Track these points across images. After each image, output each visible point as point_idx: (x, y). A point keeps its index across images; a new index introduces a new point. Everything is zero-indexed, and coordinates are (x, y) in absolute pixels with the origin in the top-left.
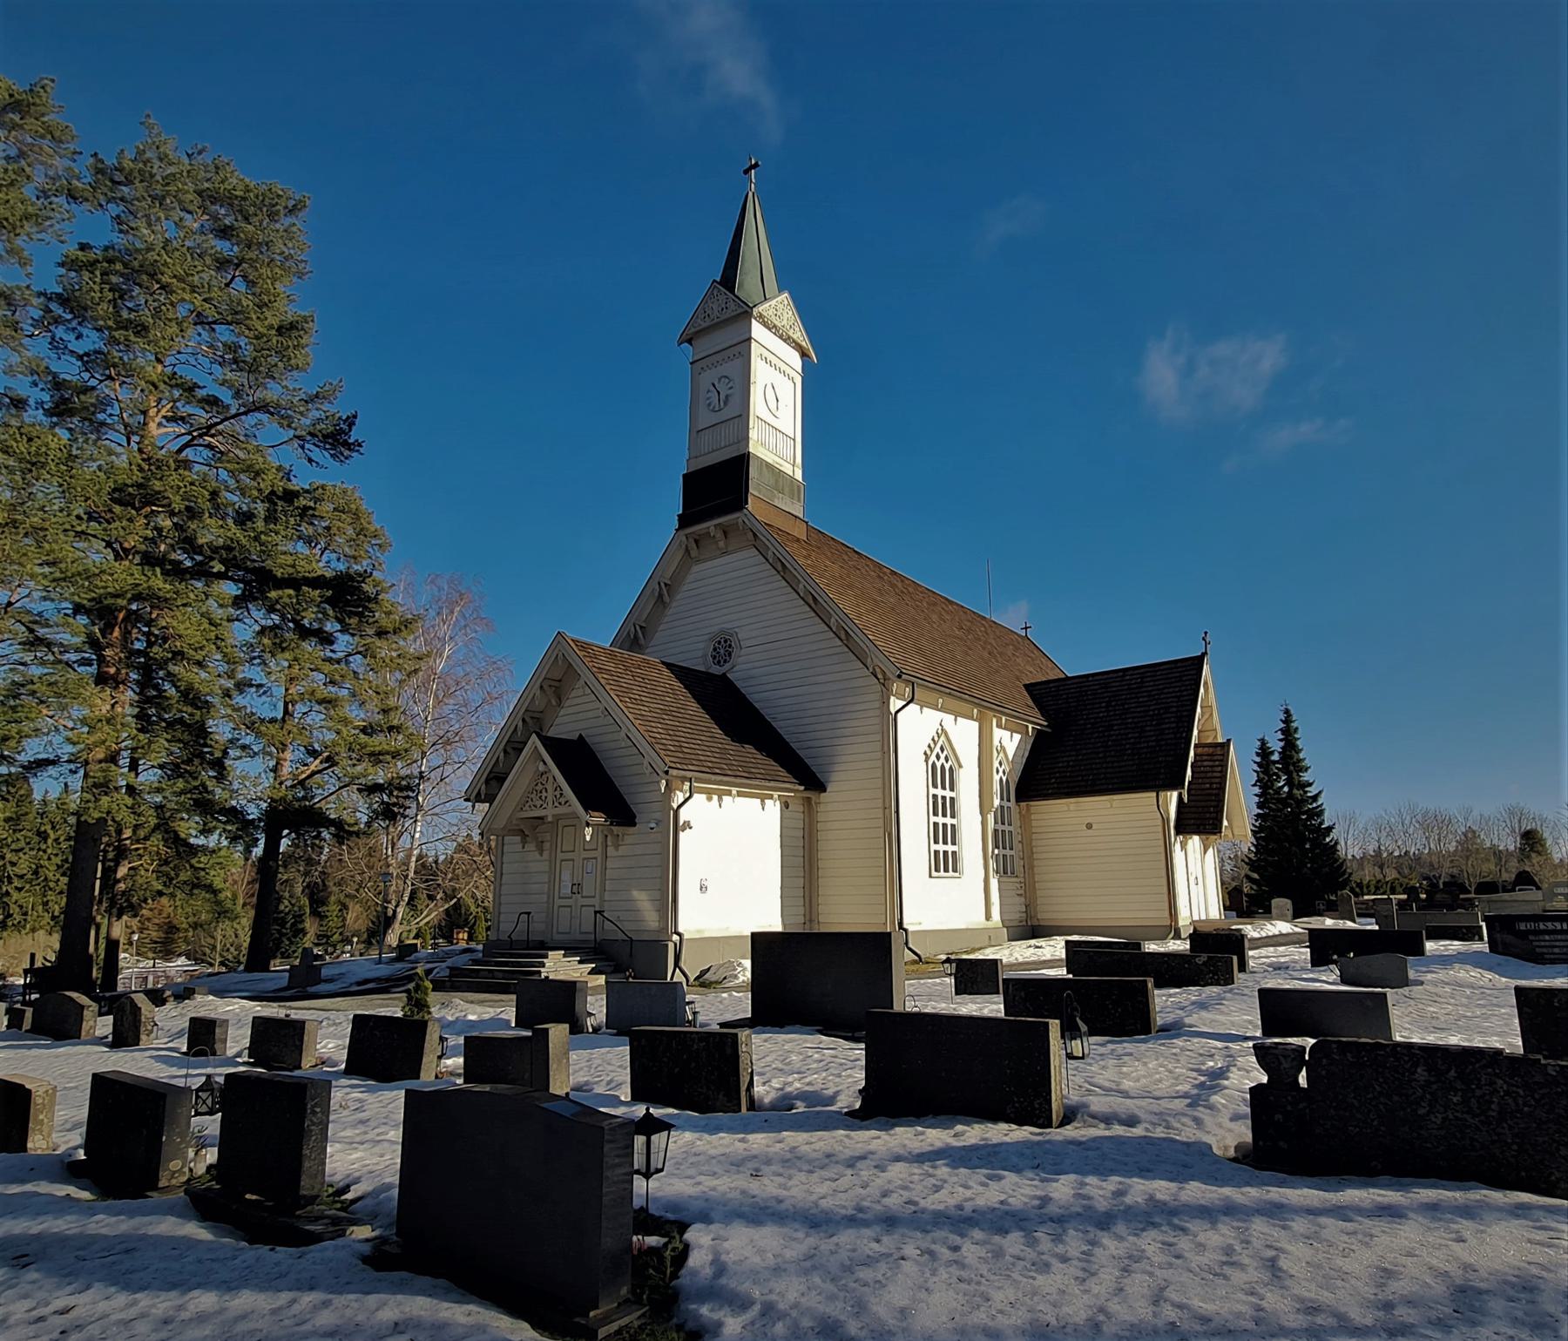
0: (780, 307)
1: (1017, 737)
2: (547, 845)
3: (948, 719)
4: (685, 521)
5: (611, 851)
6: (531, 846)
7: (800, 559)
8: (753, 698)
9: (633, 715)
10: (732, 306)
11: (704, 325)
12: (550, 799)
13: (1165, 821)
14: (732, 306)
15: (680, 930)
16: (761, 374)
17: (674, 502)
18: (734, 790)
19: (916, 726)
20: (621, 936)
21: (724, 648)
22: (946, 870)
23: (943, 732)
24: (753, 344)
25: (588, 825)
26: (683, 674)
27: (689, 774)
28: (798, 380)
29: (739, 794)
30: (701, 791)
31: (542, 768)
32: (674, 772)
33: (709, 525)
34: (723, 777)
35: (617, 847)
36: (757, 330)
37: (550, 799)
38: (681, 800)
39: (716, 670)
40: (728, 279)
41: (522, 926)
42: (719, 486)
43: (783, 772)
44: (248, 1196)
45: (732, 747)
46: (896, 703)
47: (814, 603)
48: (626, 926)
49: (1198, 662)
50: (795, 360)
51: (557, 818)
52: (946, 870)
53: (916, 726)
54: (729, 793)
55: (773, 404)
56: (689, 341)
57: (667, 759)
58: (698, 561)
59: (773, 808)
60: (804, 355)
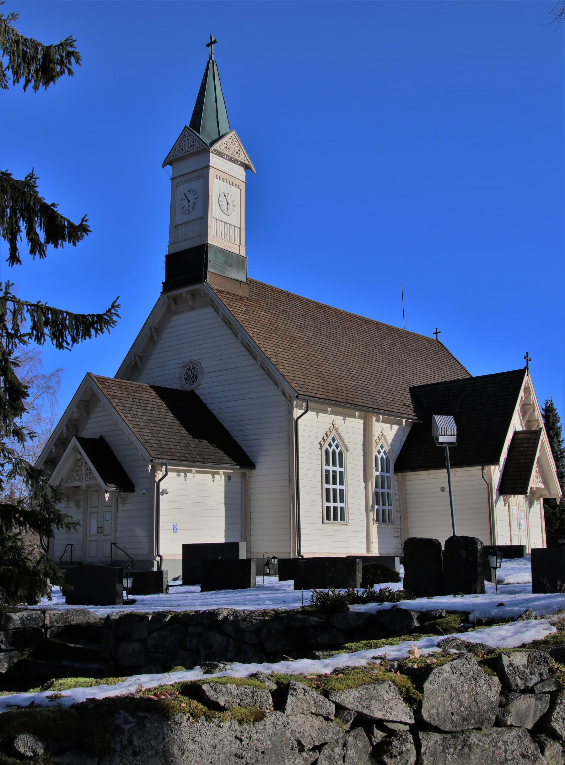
0: (230, 143)
1: (396, 427)
2: (82, 504)
3: (339, 420)
4: (167, 287)
5: (120, 507)
6: (72, 504)
7: (239, 313)
8: (211, 407)
9: (136, 423)
10: (197, 144)
11: (179, 155)
12: (84, 475)
13: (490, 486)
14: (197, 144)
15: (161, 553)
16: (216, 187)
17: (159, 274)
18: (194, 470)
19: (313, 426)
20: (126, 558)
21: (192, 372)
22: (335, 518)
23: (334, 426)
24: (211, 170)
25: (107, 492)
26: (164, 393)
27: (165, 461)
28: (243, 186)
29: (197, 472)
30: (173, 471)
31: (79, 457)
32: (156, 461)
33: (183, 291)
34: (187, 460)
35: (124, 504)
36: (214, 160)
37: (84, 475)
38: (161, 476)
39: (188, 387)
40: (196, 122)
41: (68, 554)
42: (187, 266)
43: (226, 457)
44: (107, 499)
45: (194, 442)
46: (297, 413)
47: (249, 348)
48: (129, 552)
49: (518, 375)
50: (241, 173)
51: (88, 487)
52: (335, 518)
53: (313, 426)
54: (191, 472)
55: (225, 206)
56: (170, 164)
57: (152, 453)
58: (176, 313)
59: (220, 480)
60: (247, 167)
